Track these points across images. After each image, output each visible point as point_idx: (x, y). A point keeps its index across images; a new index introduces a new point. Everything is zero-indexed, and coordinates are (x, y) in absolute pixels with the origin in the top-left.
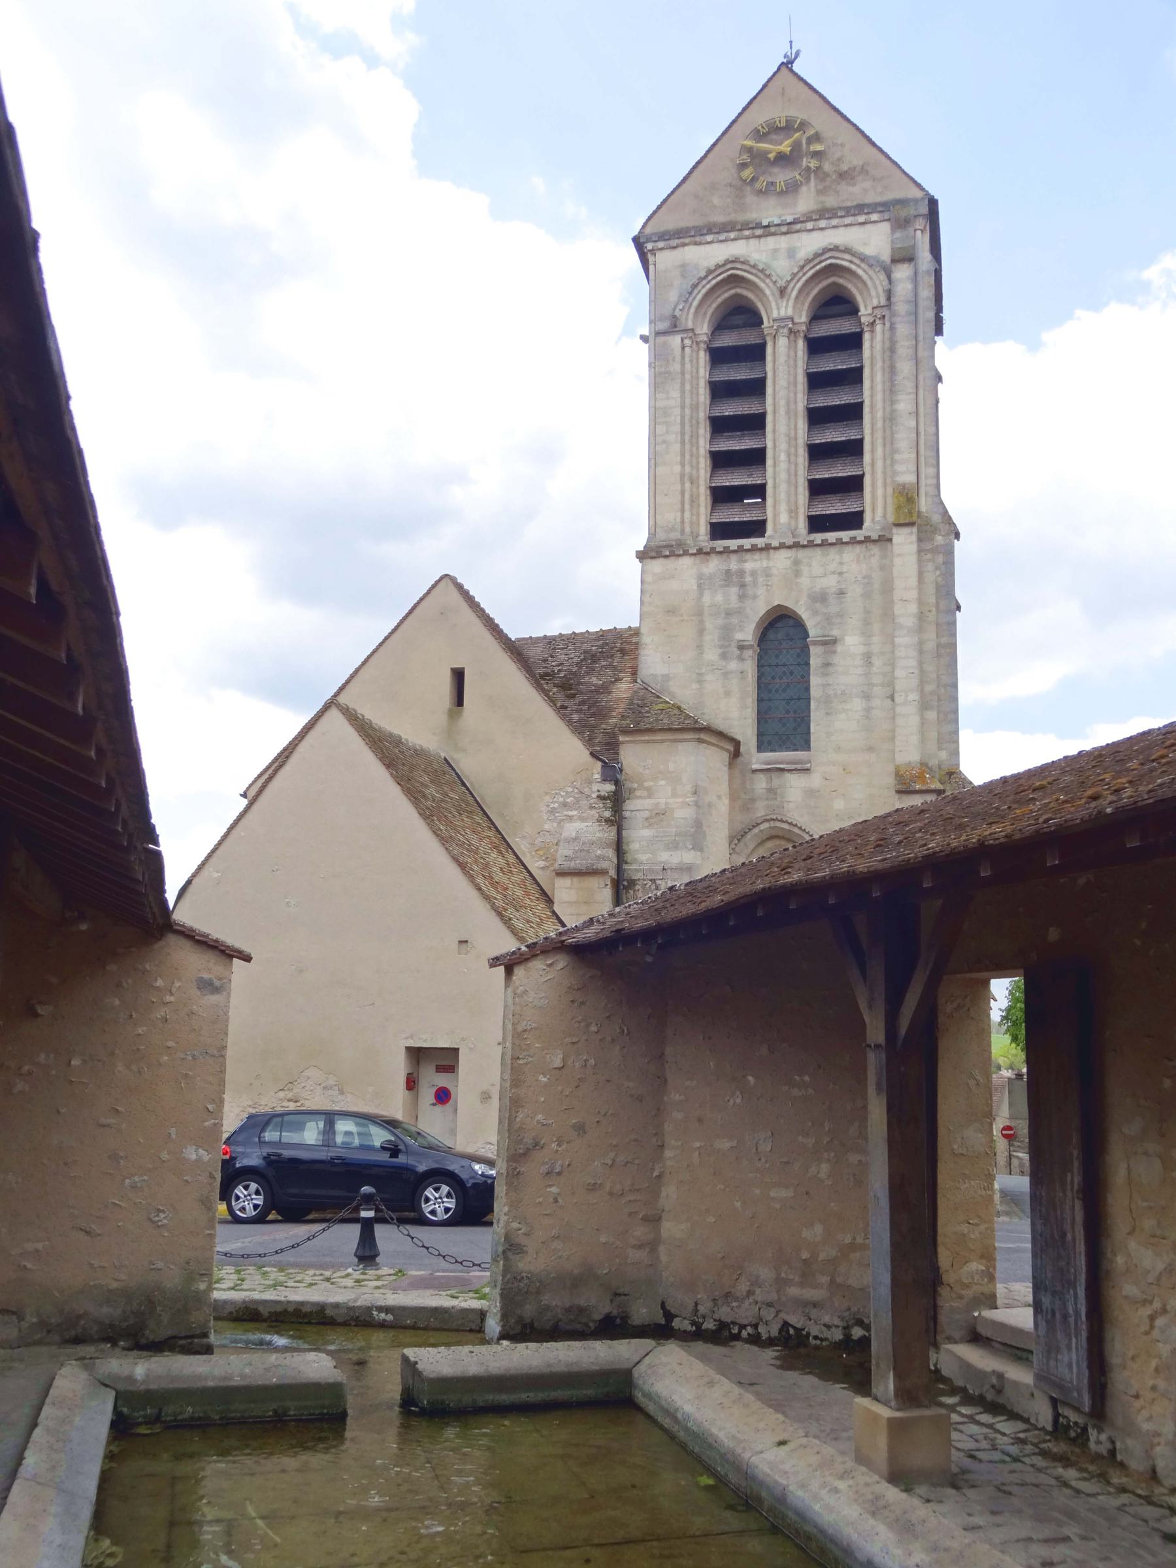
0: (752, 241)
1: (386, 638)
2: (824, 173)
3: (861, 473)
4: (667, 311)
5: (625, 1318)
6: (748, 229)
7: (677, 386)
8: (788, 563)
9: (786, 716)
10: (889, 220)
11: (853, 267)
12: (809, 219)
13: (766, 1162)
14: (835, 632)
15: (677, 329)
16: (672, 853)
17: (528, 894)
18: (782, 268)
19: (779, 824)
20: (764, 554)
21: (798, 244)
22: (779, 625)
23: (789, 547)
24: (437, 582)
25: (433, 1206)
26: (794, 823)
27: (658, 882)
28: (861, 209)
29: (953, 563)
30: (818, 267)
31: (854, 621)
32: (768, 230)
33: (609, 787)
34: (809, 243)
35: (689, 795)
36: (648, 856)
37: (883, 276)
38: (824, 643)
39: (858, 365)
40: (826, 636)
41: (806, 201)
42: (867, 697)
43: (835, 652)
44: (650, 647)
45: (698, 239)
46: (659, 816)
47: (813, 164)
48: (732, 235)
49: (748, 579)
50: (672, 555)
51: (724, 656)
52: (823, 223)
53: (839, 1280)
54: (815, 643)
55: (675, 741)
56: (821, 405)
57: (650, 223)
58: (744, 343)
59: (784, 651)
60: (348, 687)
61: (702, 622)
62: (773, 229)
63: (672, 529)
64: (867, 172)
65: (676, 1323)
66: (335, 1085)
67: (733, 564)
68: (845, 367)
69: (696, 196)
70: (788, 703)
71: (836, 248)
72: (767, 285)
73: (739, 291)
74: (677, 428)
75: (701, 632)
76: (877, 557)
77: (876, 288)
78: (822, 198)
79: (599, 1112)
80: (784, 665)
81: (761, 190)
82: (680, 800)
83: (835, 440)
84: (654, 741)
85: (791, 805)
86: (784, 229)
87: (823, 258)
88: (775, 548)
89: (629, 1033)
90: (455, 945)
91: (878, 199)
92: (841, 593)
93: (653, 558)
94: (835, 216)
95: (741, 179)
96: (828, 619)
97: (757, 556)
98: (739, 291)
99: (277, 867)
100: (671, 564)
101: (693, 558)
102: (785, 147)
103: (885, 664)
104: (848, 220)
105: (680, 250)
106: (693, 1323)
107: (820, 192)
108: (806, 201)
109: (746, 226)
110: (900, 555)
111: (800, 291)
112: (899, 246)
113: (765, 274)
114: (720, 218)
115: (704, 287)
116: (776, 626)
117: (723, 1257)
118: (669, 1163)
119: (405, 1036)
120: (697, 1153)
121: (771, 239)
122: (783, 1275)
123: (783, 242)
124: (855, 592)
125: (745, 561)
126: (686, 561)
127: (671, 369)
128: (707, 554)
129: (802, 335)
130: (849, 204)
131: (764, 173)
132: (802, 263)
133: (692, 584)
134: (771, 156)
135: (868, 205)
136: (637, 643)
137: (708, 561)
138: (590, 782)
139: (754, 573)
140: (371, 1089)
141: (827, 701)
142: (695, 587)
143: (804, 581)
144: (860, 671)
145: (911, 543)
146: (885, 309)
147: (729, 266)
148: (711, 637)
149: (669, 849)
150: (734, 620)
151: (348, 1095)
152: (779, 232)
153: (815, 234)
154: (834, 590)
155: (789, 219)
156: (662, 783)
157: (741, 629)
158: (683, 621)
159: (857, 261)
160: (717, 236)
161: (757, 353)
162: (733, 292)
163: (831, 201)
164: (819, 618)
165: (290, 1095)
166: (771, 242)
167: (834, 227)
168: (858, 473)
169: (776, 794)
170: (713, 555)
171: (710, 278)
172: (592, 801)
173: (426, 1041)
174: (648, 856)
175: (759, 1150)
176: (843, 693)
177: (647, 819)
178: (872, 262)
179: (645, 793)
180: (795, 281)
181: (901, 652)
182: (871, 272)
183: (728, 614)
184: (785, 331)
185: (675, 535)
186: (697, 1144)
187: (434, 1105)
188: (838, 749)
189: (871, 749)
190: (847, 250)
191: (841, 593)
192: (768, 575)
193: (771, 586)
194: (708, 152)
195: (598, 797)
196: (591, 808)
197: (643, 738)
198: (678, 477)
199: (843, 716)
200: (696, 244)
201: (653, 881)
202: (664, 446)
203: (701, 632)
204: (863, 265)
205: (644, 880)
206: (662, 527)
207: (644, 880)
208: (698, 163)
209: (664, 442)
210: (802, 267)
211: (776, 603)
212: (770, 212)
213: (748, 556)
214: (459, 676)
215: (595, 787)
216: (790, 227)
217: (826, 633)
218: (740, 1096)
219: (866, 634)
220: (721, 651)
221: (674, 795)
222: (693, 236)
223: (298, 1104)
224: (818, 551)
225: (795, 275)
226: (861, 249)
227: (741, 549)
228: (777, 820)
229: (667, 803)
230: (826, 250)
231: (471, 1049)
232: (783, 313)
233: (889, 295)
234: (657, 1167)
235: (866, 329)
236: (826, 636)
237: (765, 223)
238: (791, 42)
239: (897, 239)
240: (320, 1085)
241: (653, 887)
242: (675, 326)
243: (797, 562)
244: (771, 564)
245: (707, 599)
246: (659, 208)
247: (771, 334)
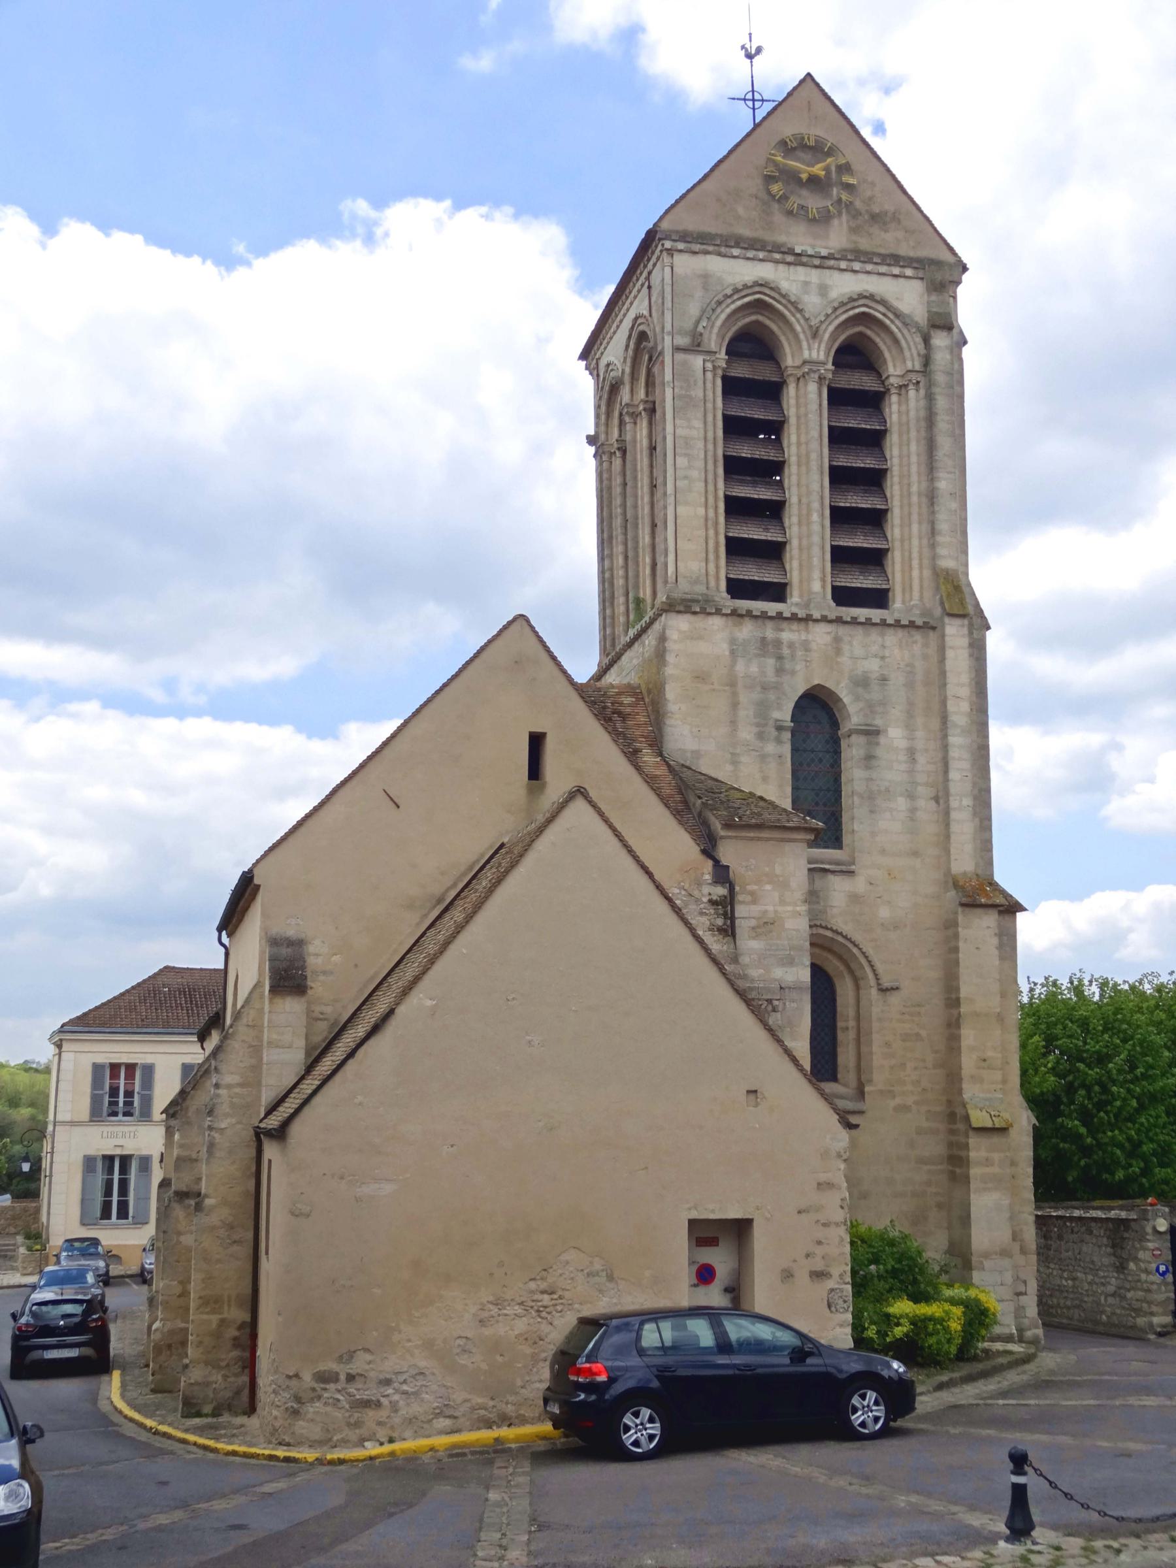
0: (781, 267)
1: (445, 685)
2: (856, 210)
4: (688, 325)
6: (779, 253)
7: (700, 415)
8: (828, 639)
10: (922, 279)
11: (887, 322)
12: (844, 258)
14: (878, 722)
15: (700, 349)
16: (785, 969)
18: (813, 303)
19: (821, 931)
20: (802, 626)
21: (829, 282)
23: (831, 622)
24: (510, 623)
25: (862, 1418)
26: (840, 931)
27: (776, 1003)
28: (895, 259)
29: (985, 660)
30: (851, 313)
31: (897, 712)
32: (798, 259)
33: (720, 891)
34: (844, 284)
35: (799, 903)
36: (761, 971)
37: (919, 339)
38: (867, 733)
41: (837, 237)
42: (911, 796)
43: (878, 744)
44: (677, 716)
45: (723, 249)
46: (766, 926)
47: (844, 196)
48: (761, 255)
49: (786, 651)
50: (704, 612)
51: (761, 736)
52: (857, 266)
55: (783, 840)
57: (668, 217)
58: (761, 378)
59: (812, 736)
60: (393, 743)
61: (735, 694)
62: (804, 259)
63: (696, 582)
64: (899, 221)
66: (603, 1270)
67: (769, 632)
68: (868, 427)
69: (719, 200)
70: (817, 795)
71: (871, 297)
72: (798, 321)
73: (760, 318)
74: (701, 464)
75: (735, 705)
76: (919, 645)
77: (910, 349)
78: (854, 238)
80: (812, 751)
81: (792, 211)
82: (790, 908)
84: (759, 839)
85: (835, 911)
86: (817, 262)
87: (856, 304)
88: (816, 621)
90: (742, 1097)
91: (912, 254)
92: (884, 679)
93: (679, 612)
94: (870, 261)
95: (769, 192)
96: (871, 707)
97: (795, 626)
98: (760, 318)
99: (513, 996)
100: (700, 622)
101: (724, 618)
102: (818, 170)
103: (928, 762)
104: (883, 269)
105: (701, 257)
107: (854, 230)
108: (837, 237)
109: (777, 248)
110: (951, 648)
111: (730, 316)
112: (934, 310)
113: (796, 308)
114: (745, 232)
115: (728, 306)
119: (687, 1206)
121: (800, 269)
123: (814, 276)
124: (897, 680)
125: (782, 630)
126: (716, 622)
127: (693, 393)
128: (741, 616)
129: (827, 382)
130: (883, 251)
131: (792, 192)
132: (836, 304)
133: (724, 648)
134: (804, 176)
135: (904, 258)
137: (741, 624)
138: (699, 884)
139: (791, 645)
140: (647, 1273)
141: (871, 797)
142: (727, 653)
143: (844, 659)
144: (903, 767)
145: (963, 636)
146: (920, 374)
147: (757, 289)
148: (746, 713)
149: (783, 965)
150: (772, 696)
151: (619, 1281)
152: (810, 264)
153: (848, 276)
154: (874, 676)
155: (824, 252)
156: (768, 887)
157: (779, 707)
159: (891, 315)
160: (744, 251)
161: (772, 392)
162: (753, 318)
163: (864, 244)
164: (861, 705)
165: (543, 1285)
166: (801, 273)
167: (868, 273)
169: (818, 897)
170: (747, 619)
171: (735, 297)
172: (702, 906)
173: (713, 1211)
174: (761, 971)
176: (887, 790)
177: (753, 928)
178: (908, 321)
179: (749, 898)
180: (827, 323)
181: (954, 753)
182: (905, 331)
183: (765, 688)
184: (816, 376)
185: (700, 589)
187: (695, 1286)
188: (883, 852)
189: (915, 854)
190: (883, 302)
191: (884, 679)
192: (807, 650)
194: (731, 152)
195: (711, 901)
196: (702, 914)
197: (748, 835)
198: (702, 520)
199: (887, 815)
200: (720, 254)
201: (770, 1001)
202: (686, 482)
203: (735, 705)
204: (897, 322)
205: (759, 1000)
206: (685, 577)
207: (759, 1000)
208: (720, 162)
209: (686, 477)
210: (835, 309)
211: (816, 682)
212: (801, 239)
213: (785, 625)
214: (536, 742)
215: (706, 889)
216: (823, 262)
217: (869, 722)
219: (909, 727)
220: (756, 730)
221: (782, 902)
222: (718, 245)
223: (555, 1296)
224: (860, 629)
225: (727, 297)
226: (896, 303)
228: (821, 926)
229: (776, 912)
230: (861, 296)
231: (767, 1219)
232: (814, 355)
233: (927, 361)
235: (893, 391)
237: (798, 250)
238: (750, 34)
239: (933, 302)
240: (582, 1270)
241: (770, 1008)
242: (699, 345)
243: (837, 640)
244: (810, 637)
245: (740, 667)
246: (677, 202)
247: (796, 375)
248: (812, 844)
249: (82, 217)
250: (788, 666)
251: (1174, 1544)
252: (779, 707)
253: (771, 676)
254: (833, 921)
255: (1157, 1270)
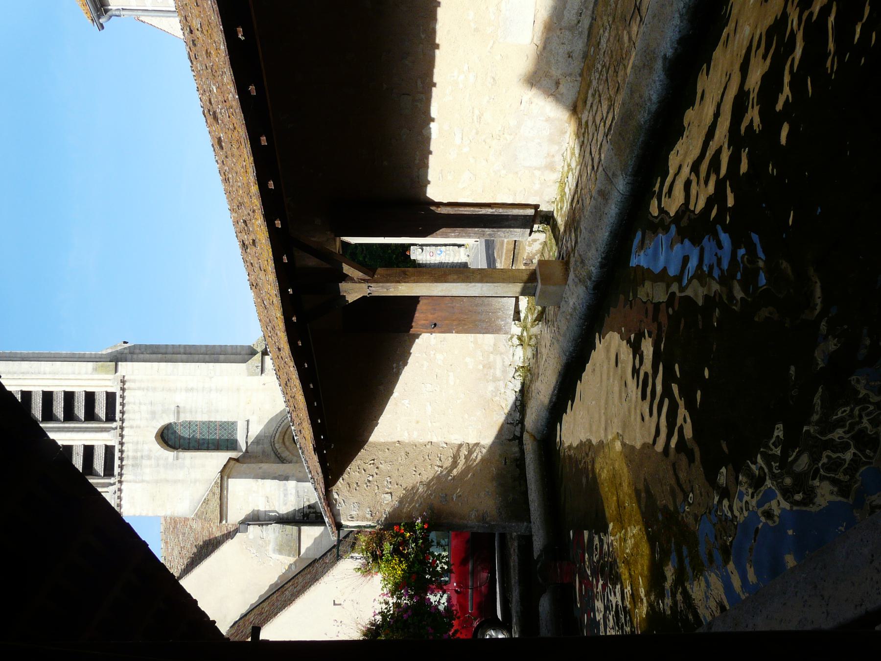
3: (84, 392)
5: (516, 460)
9: (218, 434)
13: (437, 387)
17: (310, 572)
22: (166, 438)
39: (20, 393)
40: (175, 413)
43: (184, 407)
53: (491, 349)
54: (178, 418)
56: (41, 414)
65: (518, 434)
79: (414, 475)
83: (63, 406)
89: (374, 460)
106: (517, 424)
116: (167, 440)
117: (484, 409)
118: (440, 439)
120: (434, 424)
122: (491, 378)
136: (171, 518)
150: (161, 462)
158: (159, 491)
168: (84, 394)
175: (431, 390)
186: (430, 424)
193: (143, 442)
218: (405, 401)
227: (121, 459)
234: (441, 446)
236: (175, 413)
248: (120, 426)
249: (729, 234)
250: (145, 453)
251: (769, 1)
252: (167, 459)
253: (153, 462)
254: (271, 432)
255: (439, 254)
